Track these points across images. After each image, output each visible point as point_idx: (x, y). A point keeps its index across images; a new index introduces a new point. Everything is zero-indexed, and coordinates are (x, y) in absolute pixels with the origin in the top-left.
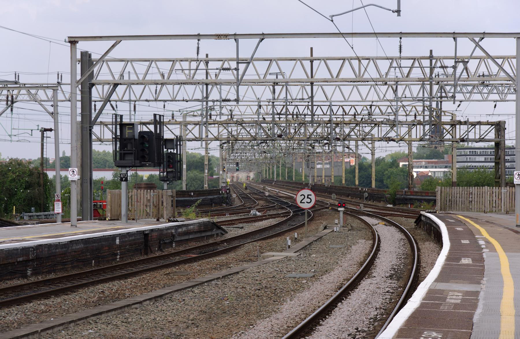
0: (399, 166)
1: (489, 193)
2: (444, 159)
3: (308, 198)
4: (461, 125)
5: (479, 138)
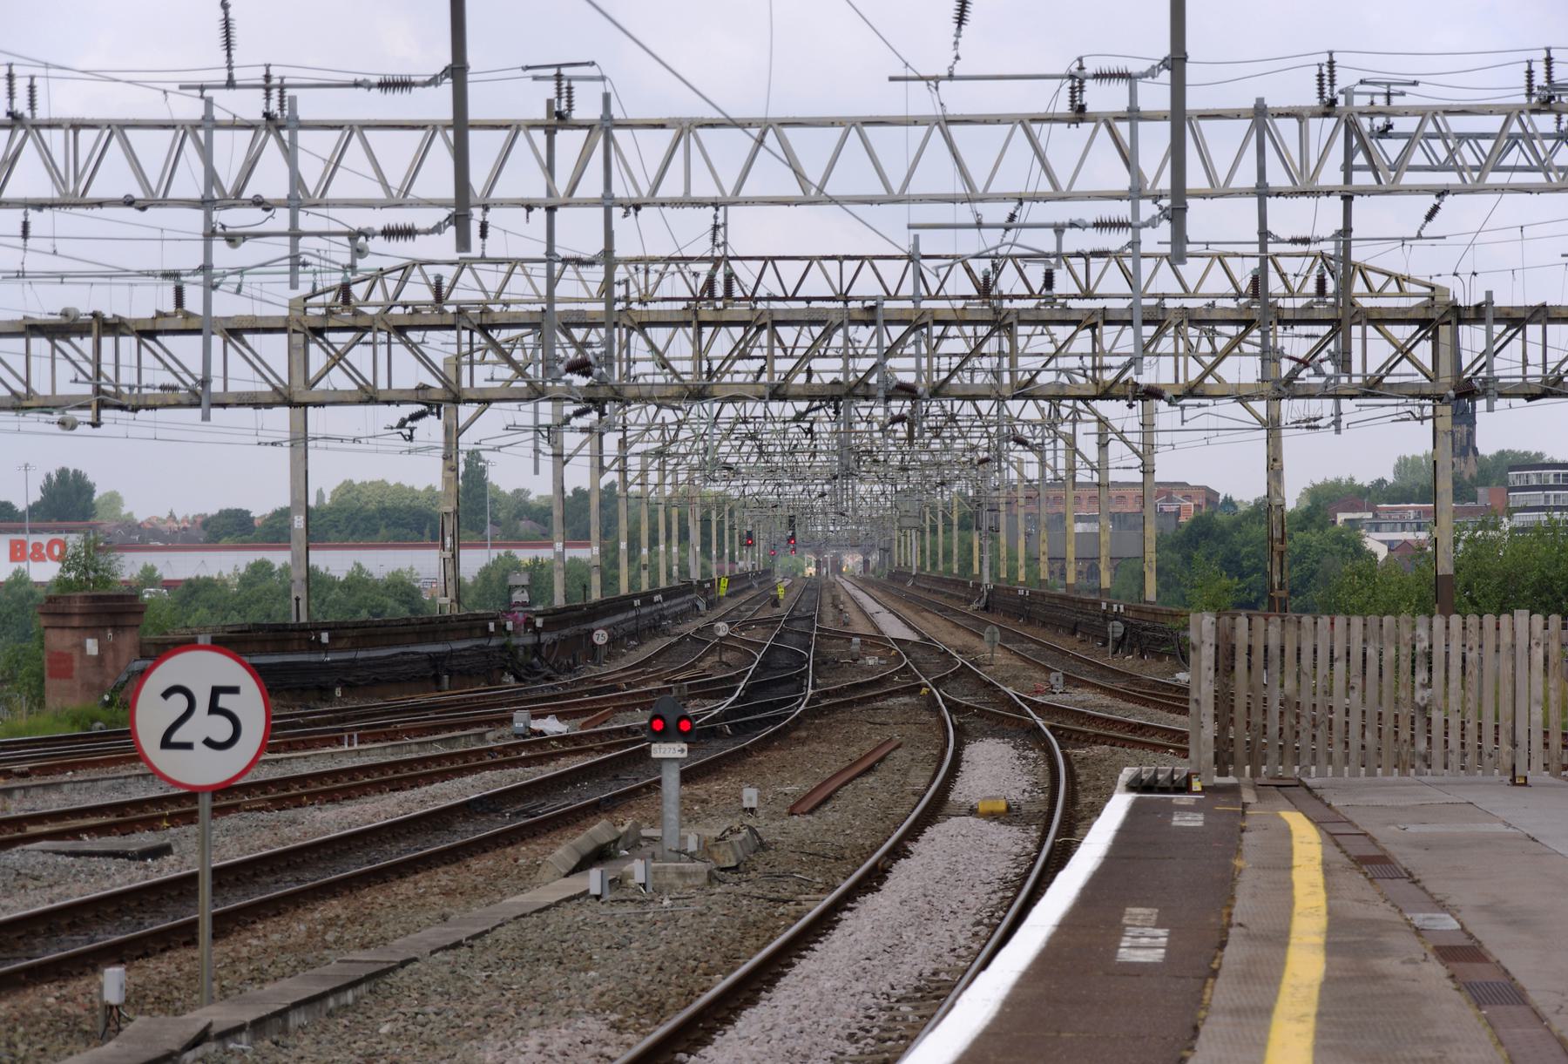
0: (1334, 522)
1: (1538, 654)
2: (1475, 500)
3: (214, 709)
4: (1461, 321)
5: (1545, 379)
